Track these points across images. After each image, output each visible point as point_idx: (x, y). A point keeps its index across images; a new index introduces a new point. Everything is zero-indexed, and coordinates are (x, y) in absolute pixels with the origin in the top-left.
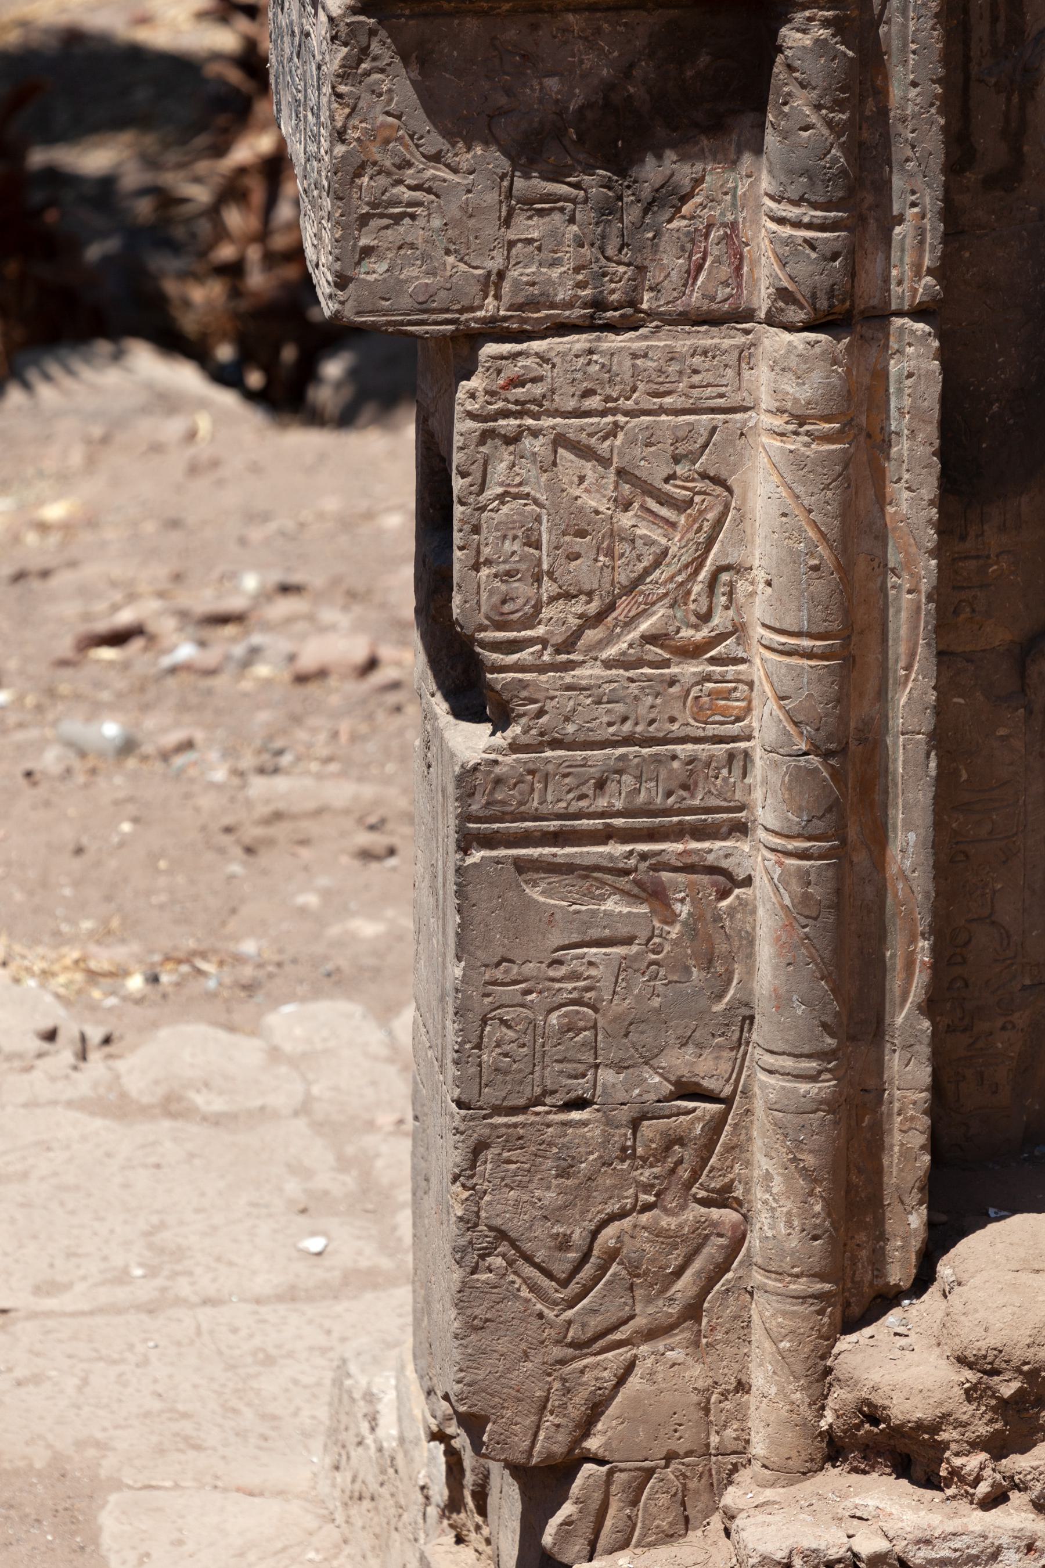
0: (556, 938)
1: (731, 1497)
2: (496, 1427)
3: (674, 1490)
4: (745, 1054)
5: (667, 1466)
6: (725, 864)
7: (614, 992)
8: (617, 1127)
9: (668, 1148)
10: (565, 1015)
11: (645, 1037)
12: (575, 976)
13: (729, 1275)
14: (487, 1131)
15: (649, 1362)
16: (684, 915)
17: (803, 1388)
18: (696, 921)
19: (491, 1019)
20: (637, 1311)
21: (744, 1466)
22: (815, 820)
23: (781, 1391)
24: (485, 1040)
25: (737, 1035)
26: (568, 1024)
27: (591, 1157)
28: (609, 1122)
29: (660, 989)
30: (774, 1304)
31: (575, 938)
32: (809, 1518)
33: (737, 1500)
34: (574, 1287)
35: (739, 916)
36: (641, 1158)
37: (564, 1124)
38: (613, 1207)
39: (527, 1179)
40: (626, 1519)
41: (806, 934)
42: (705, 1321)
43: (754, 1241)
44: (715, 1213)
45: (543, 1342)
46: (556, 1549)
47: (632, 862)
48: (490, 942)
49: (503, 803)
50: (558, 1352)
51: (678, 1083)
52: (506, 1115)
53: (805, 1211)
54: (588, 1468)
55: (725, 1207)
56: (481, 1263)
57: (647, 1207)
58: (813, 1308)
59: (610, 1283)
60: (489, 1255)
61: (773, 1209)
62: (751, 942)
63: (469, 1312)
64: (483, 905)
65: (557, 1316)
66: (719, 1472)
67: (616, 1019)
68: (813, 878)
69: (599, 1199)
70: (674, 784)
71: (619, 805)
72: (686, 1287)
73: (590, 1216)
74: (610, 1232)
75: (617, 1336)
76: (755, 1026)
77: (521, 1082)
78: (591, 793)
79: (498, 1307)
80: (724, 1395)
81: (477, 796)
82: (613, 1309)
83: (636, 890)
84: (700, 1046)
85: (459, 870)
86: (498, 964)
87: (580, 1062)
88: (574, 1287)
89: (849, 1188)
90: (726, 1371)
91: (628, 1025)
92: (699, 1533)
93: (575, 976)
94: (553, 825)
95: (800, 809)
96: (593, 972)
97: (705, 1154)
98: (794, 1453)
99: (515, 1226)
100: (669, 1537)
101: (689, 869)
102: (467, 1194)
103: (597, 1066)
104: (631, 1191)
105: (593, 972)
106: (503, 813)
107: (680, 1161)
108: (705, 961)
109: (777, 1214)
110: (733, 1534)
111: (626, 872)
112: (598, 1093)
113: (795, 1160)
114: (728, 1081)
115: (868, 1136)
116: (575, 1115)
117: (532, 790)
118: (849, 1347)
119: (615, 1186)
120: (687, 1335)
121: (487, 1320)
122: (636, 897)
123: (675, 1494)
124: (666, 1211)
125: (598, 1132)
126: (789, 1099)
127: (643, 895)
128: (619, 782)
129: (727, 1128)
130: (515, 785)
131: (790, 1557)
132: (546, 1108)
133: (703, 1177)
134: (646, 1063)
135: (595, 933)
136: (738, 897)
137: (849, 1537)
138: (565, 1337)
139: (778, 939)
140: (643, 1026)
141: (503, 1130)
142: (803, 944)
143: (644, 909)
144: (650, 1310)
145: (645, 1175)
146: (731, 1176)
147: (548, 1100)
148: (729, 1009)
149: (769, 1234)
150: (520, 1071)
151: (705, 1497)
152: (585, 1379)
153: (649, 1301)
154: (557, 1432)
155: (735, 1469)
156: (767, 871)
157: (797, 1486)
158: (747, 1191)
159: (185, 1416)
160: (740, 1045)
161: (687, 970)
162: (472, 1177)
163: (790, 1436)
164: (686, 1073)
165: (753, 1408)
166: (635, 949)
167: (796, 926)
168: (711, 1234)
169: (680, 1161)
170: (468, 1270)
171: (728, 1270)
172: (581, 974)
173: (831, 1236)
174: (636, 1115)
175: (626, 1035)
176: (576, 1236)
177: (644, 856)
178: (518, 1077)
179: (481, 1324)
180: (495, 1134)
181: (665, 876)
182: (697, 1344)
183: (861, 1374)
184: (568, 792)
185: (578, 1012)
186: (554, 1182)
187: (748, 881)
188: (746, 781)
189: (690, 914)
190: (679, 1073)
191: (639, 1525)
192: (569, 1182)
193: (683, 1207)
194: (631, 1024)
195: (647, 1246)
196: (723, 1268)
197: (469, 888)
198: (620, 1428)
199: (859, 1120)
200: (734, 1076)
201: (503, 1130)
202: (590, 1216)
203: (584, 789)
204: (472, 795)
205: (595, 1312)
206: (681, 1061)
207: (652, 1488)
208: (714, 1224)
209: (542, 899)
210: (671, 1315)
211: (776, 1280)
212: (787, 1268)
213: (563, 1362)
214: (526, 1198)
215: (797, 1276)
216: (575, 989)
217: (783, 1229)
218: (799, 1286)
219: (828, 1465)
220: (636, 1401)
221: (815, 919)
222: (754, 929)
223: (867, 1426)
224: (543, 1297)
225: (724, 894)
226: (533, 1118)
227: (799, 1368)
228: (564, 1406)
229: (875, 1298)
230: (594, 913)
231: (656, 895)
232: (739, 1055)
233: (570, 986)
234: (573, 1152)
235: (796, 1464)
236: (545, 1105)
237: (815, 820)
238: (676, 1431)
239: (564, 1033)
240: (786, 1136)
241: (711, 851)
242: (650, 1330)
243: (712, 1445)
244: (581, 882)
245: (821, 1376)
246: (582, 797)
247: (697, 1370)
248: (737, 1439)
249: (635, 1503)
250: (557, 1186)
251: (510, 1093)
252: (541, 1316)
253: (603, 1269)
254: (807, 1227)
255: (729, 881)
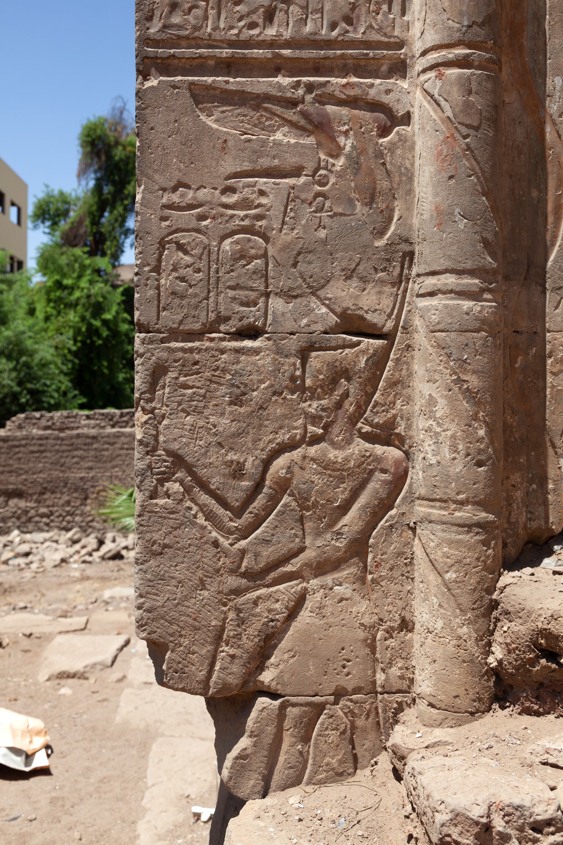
0: (229, 165)
1: (399, 736)
2: (174, 656)
3: (342, 727)
4: (405, 291)
5: (336, 703)
6: (385, 99)
7: (283, 223)
8: (286, 356)
9: (334, 382)
10: (237, 242)
11: (312, 267)
12: (245, 204)
13: (393, 512)
14: (165, 355)
15: (318, 596)
16: (348, 148)
17: (470, 622)
18: (359, 154)
19: (169, 242)
20: (307, 543)
21: (409, 706)
22: (475, 27)
23: (447, 624)
24: (163, 264)
25: (398, 270)
26: (241, 250)
27: (263, 386)
28: (279, 351)
29: (326, 221)
30: (440, 534)
31: (247, 166)
32: (493, 763)
33: (407, 740)
34: (247, 517)
35: (399, 152)
36: (310, 388)
37: (238, 351)
38: (283, 437)
39: (202, 404)
40: (297, 754)
41: (467, 144)
42: (370, 556)
43: (417, 476)
44: (379, 449)
45: (218, 571)
46: (231, 783)
47: (301, 92)
48: (168, 165)
49: (180, 27)
50: (233, 582)
51: (344, 315)
52: (182, 341)
53: (469, 437)
54: (263, 701)
55: (389, 444)
56: (159, 488)
57: (316, 440)
58: (478, 538)
59: (281, 513)
60: (168, 480)
61: (437, 434)
62: (411, 179)
63: (148, 536)
64: (159, 128)
65: (231, 545)
66: (385, 711)
67: (285, 248)
68: (474, 86)
69: (270, 429)
70: (337, 16)
71: (287, 34)
72: (352, 522)
73: (261, 445)
74: (280, 463)
75: (288, 568)
76: (416, 260)
77: (196, 307)
78: (260, 21)
79: (175, 533)
80: (390, 632)
81: (156, 20)
82: (284, 540)
83: (303, 122)
84: (364, 280)
85: (139, 94)
86: (174, 189)
87: (252, 289)
88: (247, 517)
89: (506, 427)
90: (390, 608)
91: (298, 255)
92: (367, 772)
93: (245, 204)
94: (226, 52)
95: (461, 14)
96: (263, 200)
97: (369, 389)
98: (461, 692)
99: (191, 452)
100: (338, 776)
101: (353, 102)
102: (146, 417)
103: (267, 295)
104: (301, 421)
105: (263, 200)
106: (179, 37)
107: (346, 395)
108: (368, 196)
109: (441, 439)
110: (406, 776)
111: (293, 103)
112: (269, 322)
113: (459, 381)
114: (389, 316)
115: (521, 377)
116: (248, 343)
117: (206, 18)
118: (515, 580)
119: (285, 416)
120: (353, 570)
121: (166, 546)
122: (303, 129)
123: (344, 732)
124: (333, 444)
125: (269, 359)
126: (452, 317)
127: (309, 127)
128: (287, 12)
129: (390, 363)
130: (190, 9)
131: (488, 816)
132: (221, 335)
133: (368, 412)
134: (313, 294)
135: (265, 162)
136: (398, 132)
137: (553, 789)
138: (239, 567)
139: (440, 153)
140: (310, 257)
141: (180, 354)
142: (465, 155)
143: (310, 140)
144: (319, 543)
145: (313, 407)
146: (394, 412)
147: (222, 328)
148: (390, 244)
149: (433, 461)
150: (196, 295)
151: (372, 735)
152: (258, 610)
153: (318, 534)
154: (231, 662)
155: (400, 709)
156: (428, 106)
157: (467, 727)
158: (409, 427)
159: (190, 714)
160: (401, 282)
161: (351, 202)
162: (151, 400)
163: (458, 673)
164: (350, 305)
165: (417, 646)
166: (303, 179)
167: (457, 135)
168: (376, 469)
169: (346, 395)
170: (147, 494)
171: (391, 507)
172: (253, 201)
173: (493, 464)
174: (304, 345)
175: (295, 265)
176: (248, 465)
177: (310, 88)
178: (194, 301)
179: (159, 550)
180: (172, 357)
181: (330, 108)
182: (363, 580)
183: (532, 603)
184: (240, 20)
185: (249, 240)
186: (228, 409)
187: (407, 119)
188: (405, 18)
189: (353, 147)
190: (344, 305)
191: (310, 761)
192: (242, 410)
193: (349, 442)
194: (299, 254)
195: (315, 478)
196: (384, 505)
197: (148, 111)
198: (291, 661)
199: (513, 361)
200: (396, 311)
201: (180, 354)
202: (261, 445)
203: (254, 18)
204: (150, 18)
205: (267, 542)
206: (343, 293)
207: (323, 724)
208: (378, 459)
209: (215, 126)
210: (338, 549)
211: (441, 508)
212: (452, 495)
213: (238, 592)
214: (201, 423)
215: (462, 503)
216: (246, 216)
217: (446, 453)
218: (465, 514)
219: (495, 706)
220: (306, 635)
221: (476, 129)
222: (413, 165)
223: (543, 661)
224: (219, 526)
225: (384, 131)
226: (208, 344)
227: (466, 600)
228: (238, 636)
229: (526, 543)
230: (264, 143)
231: (320, 127)
232: (400, 292)
233: (242, 213)
234: (245, 379)
235: (464, 703)
236: (220, 332)
237: (475, 27)
238: (344, 667)
239: (236, 260)
240: (449, 356)
241: (372, 85)
242: (319, 563)
243: (379, 682)
244: (252, 113)
245: (488, 610)
246: (252, 25)
247: (363, 606)
248: (402, 677)
249: (306, 739)
250: (231, 413)
251: (186, 317)
252: (216, 544)
253: (274, 500)
254: (472, 451)
255: (392, 119)
